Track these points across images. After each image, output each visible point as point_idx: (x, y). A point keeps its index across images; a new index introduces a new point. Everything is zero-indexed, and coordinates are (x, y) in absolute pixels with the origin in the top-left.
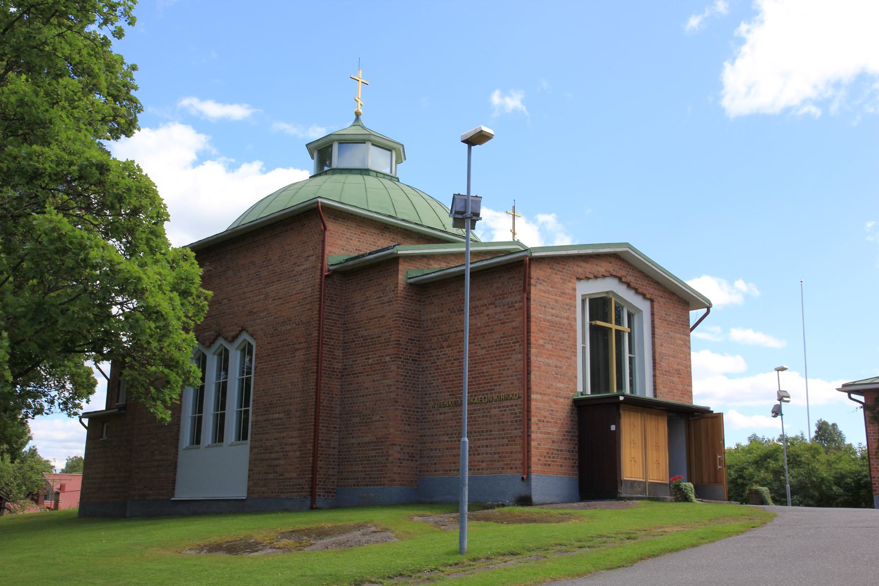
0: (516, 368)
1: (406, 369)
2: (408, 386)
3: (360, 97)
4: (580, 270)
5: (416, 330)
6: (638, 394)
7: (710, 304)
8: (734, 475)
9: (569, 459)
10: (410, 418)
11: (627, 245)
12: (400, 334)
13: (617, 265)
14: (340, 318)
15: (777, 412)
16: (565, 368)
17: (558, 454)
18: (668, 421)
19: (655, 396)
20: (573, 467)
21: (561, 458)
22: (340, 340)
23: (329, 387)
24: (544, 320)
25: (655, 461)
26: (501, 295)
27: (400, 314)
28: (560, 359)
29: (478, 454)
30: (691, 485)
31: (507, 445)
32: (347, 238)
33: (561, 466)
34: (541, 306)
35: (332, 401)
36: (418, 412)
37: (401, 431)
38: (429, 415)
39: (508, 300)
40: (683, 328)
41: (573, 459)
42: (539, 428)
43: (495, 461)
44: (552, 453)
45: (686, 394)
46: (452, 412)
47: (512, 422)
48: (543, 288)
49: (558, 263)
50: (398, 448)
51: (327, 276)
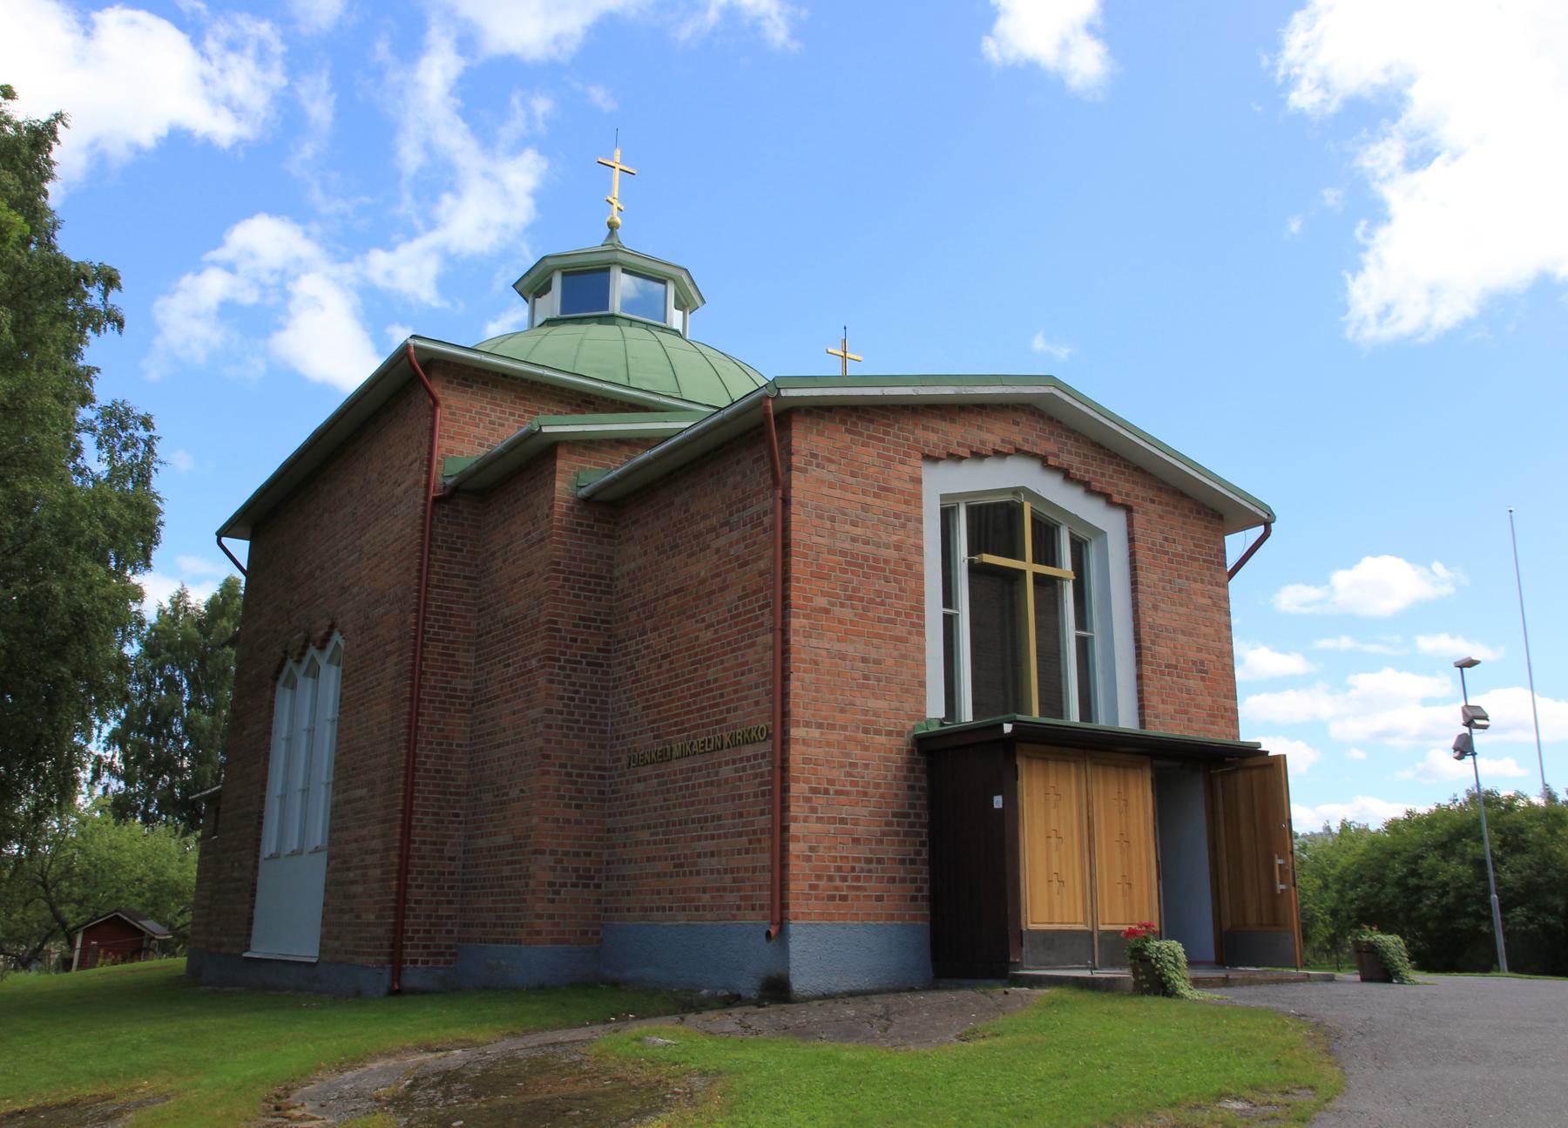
0: (764, 667)
1: (573, 684)
2: (577, 721)
3: (616, 196)
4: (934, 438)
5: (600, 599)
6: (1102, 721)
7: (1271, 514)
8: (1401, 871)
9: (903, 880)
10: (581, 791)
11: (1051, 380)
12: (556, 607)
13: (1034, 428)
14: (471, 585)
15: (1464, 748)
16: (890, 661)
17: (870, 871)
18: (1152, 779)
19: (1142, 724)
20: (914, 898)
21: (880, 880)
22: (469, 631)
23: (440, 730)
24: (831, 551)
25: (1119, 879)
26: (741, 501)
27: (558, 564)
28: (875, 641)
29: (698, 873)
30: (1177, 947)
31: (747, 851)
32: (492, 423)
33: (879, 899)
34: (820, 517)
35: (448, 759)
36: (602, 777)
37: (557, 820)
38: (622, 783)
39: (750, 511)
40: (1209, 569)
41: (914, 880)
42: (813, 810)
43: (725, 889)
44: (853, 869)
45: (1222, 717)
46: (657, 776)
47: (756, 795)
48: (829, 477)
49: (871, 421)
50: (548, 860)
51: (436, 500)
